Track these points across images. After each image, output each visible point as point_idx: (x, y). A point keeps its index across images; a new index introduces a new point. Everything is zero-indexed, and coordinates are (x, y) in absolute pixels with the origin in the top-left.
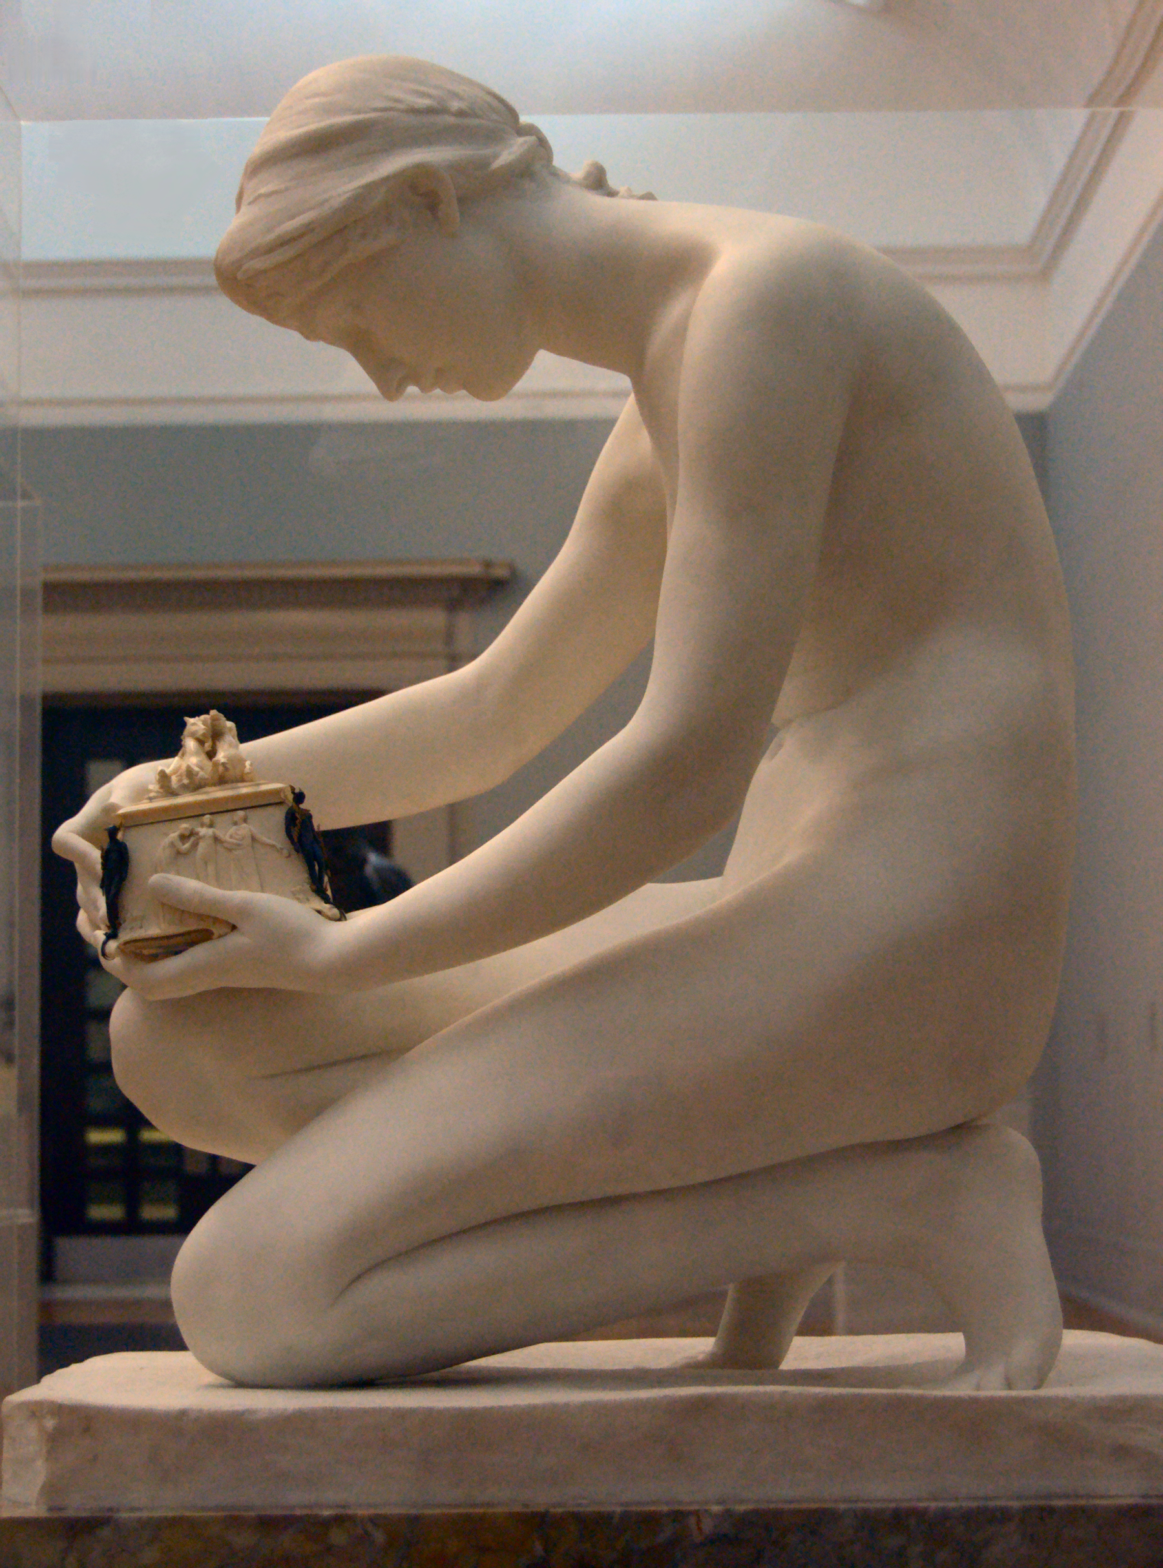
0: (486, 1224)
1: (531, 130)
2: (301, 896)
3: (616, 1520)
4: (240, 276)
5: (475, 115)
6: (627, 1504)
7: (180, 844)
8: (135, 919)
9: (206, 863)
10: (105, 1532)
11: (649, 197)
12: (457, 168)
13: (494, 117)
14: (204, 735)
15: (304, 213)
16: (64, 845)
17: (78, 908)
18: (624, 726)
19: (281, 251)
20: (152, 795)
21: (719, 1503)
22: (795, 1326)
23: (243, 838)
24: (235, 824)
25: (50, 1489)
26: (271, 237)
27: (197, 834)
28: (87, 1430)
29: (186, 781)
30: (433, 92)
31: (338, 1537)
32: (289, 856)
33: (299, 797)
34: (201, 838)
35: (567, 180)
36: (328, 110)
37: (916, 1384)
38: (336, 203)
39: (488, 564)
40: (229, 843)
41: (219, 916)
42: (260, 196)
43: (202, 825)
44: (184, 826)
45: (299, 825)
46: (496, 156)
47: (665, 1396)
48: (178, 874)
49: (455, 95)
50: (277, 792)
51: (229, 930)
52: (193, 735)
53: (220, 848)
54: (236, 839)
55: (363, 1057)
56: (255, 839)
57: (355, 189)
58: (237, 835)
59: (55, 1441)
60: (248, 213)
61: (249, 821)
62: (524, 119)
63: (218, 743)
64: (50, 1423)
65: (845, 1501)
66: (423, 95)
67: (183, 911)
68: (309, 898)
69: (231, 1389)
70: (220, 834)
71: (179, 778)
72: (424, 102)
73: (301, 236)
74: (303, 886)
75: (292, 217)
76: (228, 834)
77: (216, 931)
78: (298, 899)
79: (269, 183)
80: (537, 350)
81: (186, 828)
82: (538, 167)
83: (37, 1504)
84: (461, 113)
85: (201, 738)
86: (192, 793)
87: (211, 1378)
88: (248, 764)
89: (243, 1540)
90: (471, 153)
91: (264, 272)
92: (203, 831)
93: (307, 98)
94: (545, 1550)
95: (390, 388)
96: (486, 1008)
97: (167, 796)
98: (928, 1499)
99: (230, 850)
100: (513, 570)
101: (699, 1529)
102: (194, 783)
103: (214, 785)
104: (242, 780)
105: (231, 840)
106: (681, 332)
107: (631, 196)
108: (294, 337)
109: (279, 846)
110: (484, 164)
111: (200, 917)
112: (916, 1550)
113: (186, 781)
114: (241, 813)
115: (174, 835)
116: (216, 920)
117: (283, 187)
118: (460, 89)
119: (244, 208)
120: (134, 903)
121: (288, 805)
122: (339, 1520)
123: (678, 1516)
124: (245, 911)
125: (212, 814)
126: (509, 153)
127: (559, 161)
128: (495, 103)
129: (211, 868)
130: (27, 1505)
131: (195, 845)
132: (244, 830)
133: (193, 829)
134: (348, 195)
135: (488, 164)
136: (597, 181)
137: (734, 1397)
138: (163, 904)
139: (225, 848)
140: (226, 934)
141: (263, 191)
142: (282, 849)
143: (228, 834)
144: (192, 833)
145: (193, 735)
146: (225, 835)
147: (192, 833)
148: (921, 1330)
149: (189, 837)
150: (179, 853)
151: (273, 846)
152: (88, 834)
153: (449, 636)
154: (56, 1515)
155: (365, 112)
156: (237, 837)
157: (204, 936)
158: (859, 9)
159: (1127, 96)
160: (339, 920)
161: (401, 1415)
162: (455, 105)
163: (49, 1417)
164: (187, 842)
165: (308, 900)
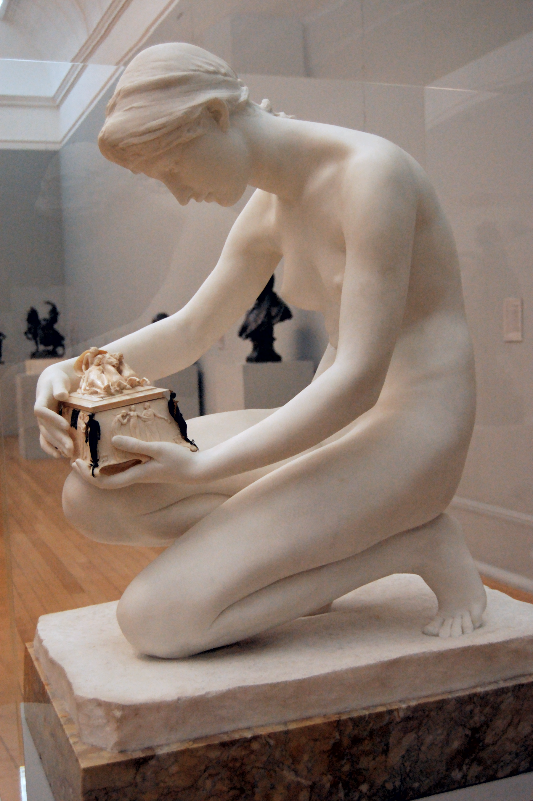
2: (177, 441)
3: (367, 717)
7: (122, 420)
8: (104, 457)
9: (135, 428)
10: (153, 762)
15: (162, 117)
19: (147, 135)
24: (145, 409)
26: (143, 128)
27: (129, 414)
30: (214, 64)
31: (255, 746)
32: (170, 423)
33: (173, 395)
34: (131, 417)
36: (168, 69)
40: (144, 418)
41: (142, 453)
43: (131, 410)
44: (123, 411)
45: (176, 408)
50: (162, 393)
54: (148, 416)
58: (147, 414)
64: (118, 714)
66: (210, 65)
68: (181, 442)
70: (139, 414)
72: (211, 68)
73: (160, 129)
74: (178, 436)
75: (154, 120)
77: (143, 460)
78: (176, 442)
81: (125, 413)
89: (214, 754)
90: (231, 94)
91: (134, 145)
92: (132, 413)
94: (340, 735)
99: (145, 421)
101: (399, 716)
109: (166, 418)
111: (134, 454)
112: (477, 710)
114: (147, 404)
115: (119, 416)
120: (103, 449)
122: (255, 738)
123: (390, 712)
129: (137, 431)
131: (129, 420)
132: (151, 411)
133: (127, 413)
134: (184, 111)
138: (117, 449)
139: (143, 421)
140: (148, 461)
141: (135, 105)
144: (127, 415)
145: (110, 364)
146: (141, 414)
147: (127, 415)
148: (359, 587)
149: (126, 416)
150: (122, 424)
151: (163, 419)
155: (186, 71)
156: (148, 415)
157: (138, 462)
159: (85, 60)
163: (116, 710)
165: (181, 442)
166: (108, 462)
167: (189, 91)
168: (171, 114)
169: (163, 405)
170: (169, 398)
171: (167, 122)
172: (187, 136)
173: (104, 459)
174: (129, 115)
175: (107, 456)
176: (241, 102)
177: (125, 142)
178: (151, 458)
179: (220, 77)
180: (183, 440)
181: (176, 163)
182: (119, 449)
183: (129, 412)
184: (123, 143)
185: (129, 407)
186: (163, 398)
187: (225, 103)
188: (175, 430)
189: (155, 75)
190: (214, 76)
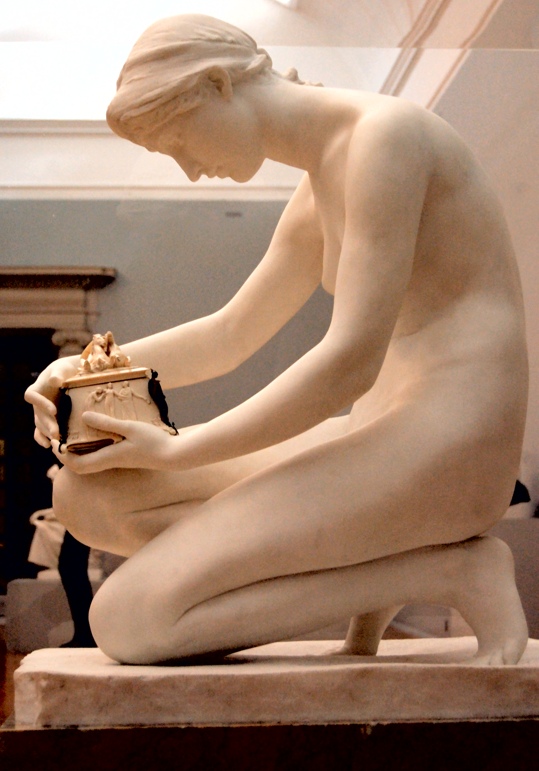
0: (248, 585)
1: (262, 52)
2: (156, 423)
4: (122, 119)
5: (239, 43)
6: (329, 721)
11: (320, 85)
12: (233, 69)
13: (247, 44)
14: (105, 344)
16: (31, 398)
17: (35, 427)
18: (319, 341)
19: (143, 107)
20: (81, 373)
21: (374, 720)
22: (381, 636)
23: (127, 395)
24: (124, 387)
25: (45, 716)
26: (139, 100)
27: (105, 392)
28: (62, 686)
29: (98, 366)
32: (150, 403)
33: (155, 374)
34: (106, 394)
35: (280, 76)
36: (167, 39)
37: (444, 662)
38: (174, 84)
39: (104, 270)
40: (121, 397)
42: (133, 80)
43: (107, 388)
44: (99, 388)
46: (249, 63)
47: (347, 669)
48: (96, 411)
49: (230, 34)
50: (144, 372)
51: (122, 439)
52: (98, 344)
53: (116, 398)
54: (124, 395)
55: (181, 502)
56: (134, 395)
57: (181, 78)
58: (125, 392)
59: (47, 692)
60: (124, 89)
61: (130, 385)
62: (259, 47)
63: (110, 347)
64: (44, 683)
65: (436, 719)
66: (216, 33)
67: (98, 430)
69: (115, 666)
70: (116, 392)
71: (94, 365)
75: (150, 91)
76: (120, 392)
77: (115, 440)
78: (155, 425)
79: (137, 74)
80: (265, 158)
81: (100, 389)
82: (267, 69)
83: (37, 723)
84: (232, 42)
85: (103, 345)
86: (101, 372)
87: (108, 660)
88: (129, 358)
91: (132, 118)
92: (108, 391)
93: (157, 33)
95: (193, 175)
96: (244, 480)
97: (88, 373)
98: (474, 718)
99: (121, 400)
100: (115, 270)
102: (102, 367)
103: (111, 368)
104: (124, 366)
105: (122, 396)
106: (344, 150)
107: (311, 85)
108: (144, 150)
109: (145, 398)
110: (243, 67)
111: (108, 433)
113: (98, 366)
114: (126, 382)
115: (94, 393)
116: (115, 434)
117: (145, 76)
118: (230, 30)
119: (122, 87)
120: (75, 426)
121: (149, 378)
124: (131, 430)
125: (112, 382)
126: (255, 62)
127: (275, 67)
128: (246, 37)
129: (112, 409)
130: (30, 724)
131: (104, 398)
132: (128, 390)
135: (246, 67)
136: (294, 77)
137: (381, 669)
138: (88, 426)
139: (119, 399)
141: (136, 77)
142: (146, 400)
143: (120, 392)
145: (98, 344)
146: (119, 393)
149: (102, 393)
150: (96, 401)
151: (142, 399)
152: (44, 392)
153: (85, 303)
154: (46, 729)
156: (125, 394)
157: (108, 443)
158: (284, 7)
160: (176, 435)
161: (218, 678)
162: (230, 38)
163: (43, 680)
164: (101, 396)
165: (160, 425)
166: (79, 439)
167: (186, 61)
168: (167, 84)
169: (144, 385)
170: (150, 377)
171: (161, 93)
172: (184, 107)
173: (74, 437)
174: (130, 87)
175: (77, 433)
176: (248, 71)
177: (124, 115)
178: (124, 438)
179: (226, 45)
180: (162, 422)
181: (179, 136)
182: (91, 427)
183: (105, 390)
184: (122, 117)
185: (106, 384)
186: (145, 377)
187: (227, 72)
188: (153, 412)
189: (154, 46)
190: (233, 46)
